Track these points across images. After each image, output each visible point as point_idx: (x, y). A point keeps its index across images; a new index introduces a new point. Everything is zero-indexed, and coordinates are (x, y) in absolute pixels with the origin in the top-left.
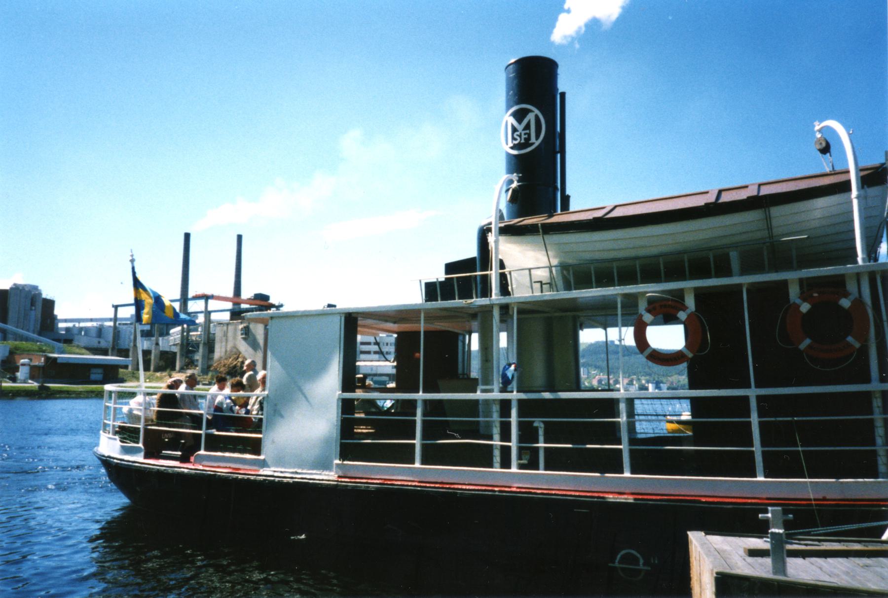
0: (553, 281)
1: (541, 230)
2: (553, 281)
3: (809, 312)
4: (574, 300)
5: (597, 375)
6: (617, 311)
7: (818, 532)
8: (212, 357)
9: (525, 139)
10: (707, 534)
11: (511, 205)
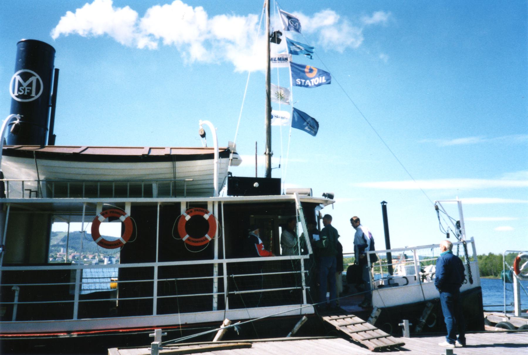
0: (39, 189)
1: (34, 156)
2: (39, 189)
3: (190, 220)
4: (51, 204)
5: (72, 253)
6: (82, 213)
7: (179, 341)
9: (28, 92)
10: (119, 349)
11: (13, 135)
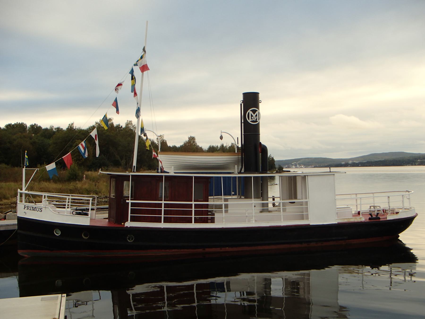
8: (92, 170)
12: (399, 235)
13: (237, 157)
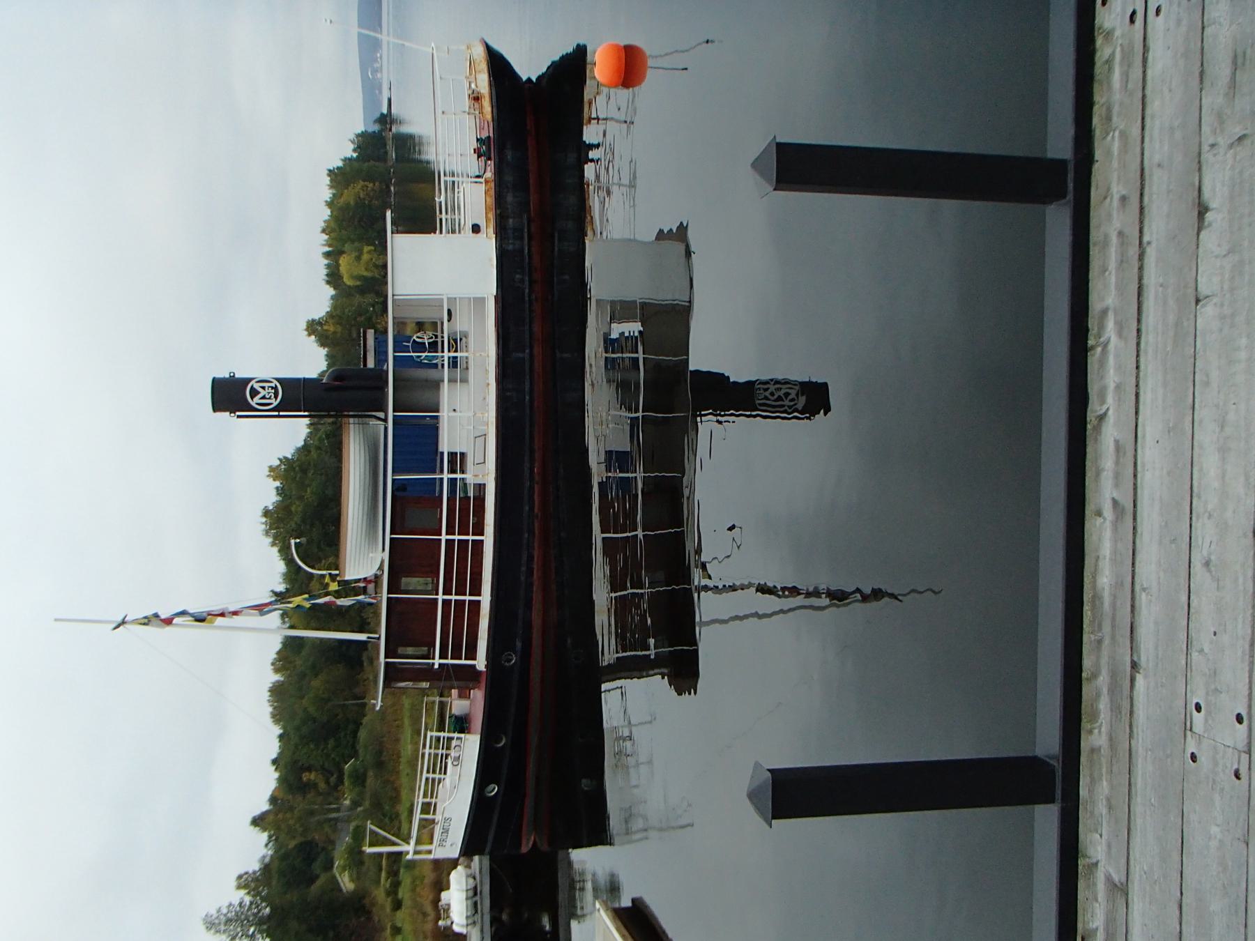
12: (524, 79)
13: (352, 426)
